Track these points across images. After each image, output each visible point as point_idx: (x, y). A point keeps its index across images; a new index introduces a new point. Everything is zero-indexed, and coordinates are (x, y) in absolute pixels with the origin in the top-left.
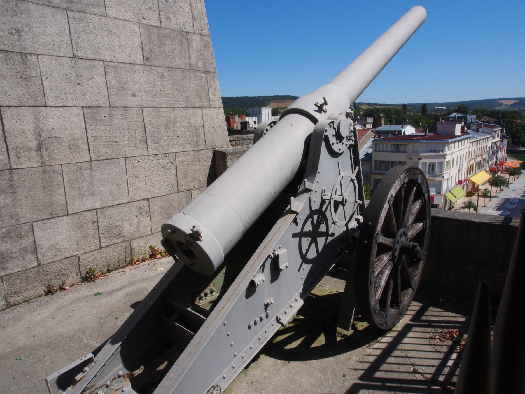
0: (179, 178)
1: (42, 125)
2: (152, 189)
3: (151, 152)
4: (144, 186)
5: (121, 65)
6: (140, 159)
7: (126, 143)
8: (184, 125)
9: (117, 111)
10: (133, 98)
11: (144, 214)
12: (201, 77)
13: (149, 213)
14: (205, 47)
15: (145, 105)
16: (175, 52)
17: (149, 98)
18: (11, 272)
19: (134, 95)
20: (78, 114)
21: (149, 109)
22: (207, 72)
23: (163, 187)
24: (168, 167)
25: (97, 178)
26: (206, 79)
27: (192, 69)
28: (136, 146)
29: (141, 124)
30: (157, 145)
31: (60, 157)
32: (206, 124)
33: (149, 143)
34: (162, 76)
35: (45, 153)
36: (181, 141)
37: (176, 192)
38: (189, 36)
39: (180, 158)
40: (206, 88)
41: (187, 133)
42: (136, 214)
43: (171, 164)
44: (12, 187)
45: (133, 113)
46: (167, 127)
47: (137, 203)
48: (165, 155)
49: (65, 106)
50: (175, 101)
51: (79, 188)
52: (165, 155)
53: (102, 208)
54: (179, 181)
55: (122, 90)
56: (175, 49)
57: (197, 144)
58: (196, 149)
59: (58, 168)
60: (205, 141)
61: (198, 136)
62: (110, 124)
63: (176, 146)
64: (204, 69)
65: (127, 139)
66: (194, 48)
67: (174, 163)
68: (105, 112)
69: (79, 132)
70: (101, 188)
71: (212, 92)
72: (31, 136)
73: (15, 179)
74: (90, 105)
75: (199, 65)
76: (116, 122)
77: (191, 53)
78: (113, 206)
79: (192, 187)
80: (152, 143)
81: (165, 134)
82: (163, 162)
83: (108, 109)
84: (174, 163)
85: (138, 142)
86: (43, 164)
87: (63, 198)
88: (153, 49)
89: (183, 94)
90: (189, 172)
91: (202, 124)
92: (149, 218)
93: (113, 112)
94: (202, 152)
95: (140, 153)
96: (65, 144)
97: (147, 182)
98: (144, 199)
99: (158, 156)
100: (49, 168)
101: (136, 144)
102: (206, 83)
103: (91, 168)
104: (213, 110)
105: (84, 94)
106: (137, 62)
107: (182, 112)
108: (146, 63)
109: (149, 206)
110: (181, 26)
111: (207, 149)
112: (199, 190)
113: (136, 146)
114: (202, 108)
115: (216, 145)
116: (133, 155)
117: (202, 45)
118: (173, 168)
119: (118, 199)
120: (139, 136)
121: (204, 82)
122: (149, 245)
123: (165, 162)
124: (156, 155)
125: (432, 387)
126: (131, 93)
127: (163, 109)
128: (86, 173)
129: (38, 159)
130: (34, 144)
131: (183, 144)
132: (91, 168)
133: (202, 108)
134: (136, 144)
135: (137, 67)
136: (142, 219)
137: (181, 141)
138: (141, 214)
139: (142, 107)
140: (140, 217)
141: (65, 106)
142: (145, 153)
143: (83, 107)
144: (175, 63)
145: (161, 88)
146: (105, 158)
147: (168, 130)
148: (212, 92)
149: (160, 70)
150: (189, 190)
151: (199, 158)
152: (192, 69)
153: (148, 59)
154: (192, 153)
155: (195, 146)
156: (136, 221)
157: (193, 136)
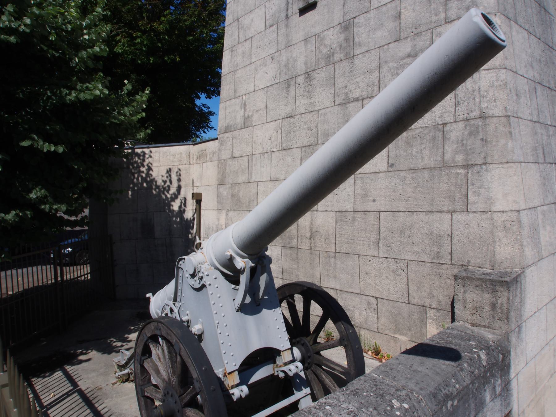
0: (411, 288)
1: (313, 223)
2: (381, 289)
3: (381, 255)
4: (374, 285)
5: (367, 175)
6: (371, 258)
7: (361, 242)
8: (422, 231)
9: (359, 215)
10: (373, 203)
11: (372, 310)
12: (458, 174)
13: (377, 310)
14: (470, 134)
15: (383, 209)
16: (424, 152)
17: (387, 203)
18: (428, 326)
19: (374, 201)
20: (333, 217)
21: (386, 213)
22: (467, 166)
23: (392, 289)
24: (398, 273)
25: (338, 266)
26: (467, 175)
27: (445, 166)
28: (369, 246)
29: (376, 227)
30: (389, 248)
31: (320, 245)
32: (455, 233)
33: (381, 245)
34: (404, 180)
35: (313, 241)
36: (416, 249)
37: (407, 302)
38: (447, 128)
39: (413, 266)
40: (464, 186)
41: (425, 241)
42: (366, 307)
43: (402, 271)
44: (297, 258)
45: (371, 217)
46: (402, 232)
47: (367, 298)
48: (396, 260)
49: (326, 211)
50: (416, 205)
51: (327, 270)
52: (396, 260)
53: (341, 291)
54: (410, 292)
55: (365, 196)
56: (425, 148)
57: (438, 255)
58: (435, 261)
59: (317, 252)
60: (451, 254)
61: (441, 246)
62: (352, 225)
63: (409, 253)
64: (464, 163)
65: (362, 239)
66: (451, 140)
67: (406, 270)
68: (350, 215)
69: (332, 230)
70: (341, 275)
71: (474, 192)
72: (308, 230)
73: (299, 254)
74: (341, 210)
75: (456, 160)
76: (356, 224)
77: (446, 148)
78: (348, 292)
79: (427, 304)
80: (383, 245)
81: (399, 239)
82: (393, 266)
83: (352, 213)
84: (406, 270)
85: (372, 243)
86: (311, 249)
87: (319, 274)
88: (398, 155)
89: (427, 196)
90: (424, 286)
91: (450, 233)
92: (376, 316)
93: (356, 215)
94: (444, 267)
95: (371, 253)
96: (323, 237)
97: (377, 281)
98: (373, 296)
99: (389, 259)
100: (313, 252)
101: (369, 245)
102: (465, 181)
103: (335, 257)
104: (471, 215)
105: (338, 202)
106: (381, 170)
107: (423, 216)
108: (390, 169)
109: (377, 305)
110: (437, 119)
111: (452, 264)
112: (438, 312)
113: (369, 246)
114: (452, 212)
115: (469, 262)
116: (366, 254)
117: (466, 133)
118: (404, 275)
119: (352, 288)
120: (373, 237)
121: (461, 180)
122: (374, 341)
123: (395, 267)
124: (386, 258)
125: (130, 197)
126: (372, 199)
127: (401, 213)
128: (332, 260)
129: (309, 244)
130: (308, 235)
131: (418, 253)
132: (335, 257)
133: (452, 212)
134: (369, 245)
135: (381, 174)
136: (370, 314)
137: (416, 249)
138: (369, 309)
139: (379, 212)
140: (368, 311)
141: (326, 211)
142: (376, 254)
143: (336, 212)
144: (422, 164)
145: (401, 192)
146: (344, 252)
147: (403, 236)
148: (474, 192)
149: (403, 174)
150: (423, 306)
151: (439, 273)
152: (445, 166)
153: (392, 165)
154: (429, 264)
155: (434, 258)
156: (365, 313)
157: (433, 245)
